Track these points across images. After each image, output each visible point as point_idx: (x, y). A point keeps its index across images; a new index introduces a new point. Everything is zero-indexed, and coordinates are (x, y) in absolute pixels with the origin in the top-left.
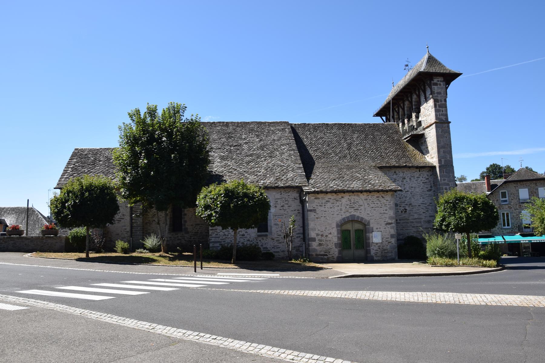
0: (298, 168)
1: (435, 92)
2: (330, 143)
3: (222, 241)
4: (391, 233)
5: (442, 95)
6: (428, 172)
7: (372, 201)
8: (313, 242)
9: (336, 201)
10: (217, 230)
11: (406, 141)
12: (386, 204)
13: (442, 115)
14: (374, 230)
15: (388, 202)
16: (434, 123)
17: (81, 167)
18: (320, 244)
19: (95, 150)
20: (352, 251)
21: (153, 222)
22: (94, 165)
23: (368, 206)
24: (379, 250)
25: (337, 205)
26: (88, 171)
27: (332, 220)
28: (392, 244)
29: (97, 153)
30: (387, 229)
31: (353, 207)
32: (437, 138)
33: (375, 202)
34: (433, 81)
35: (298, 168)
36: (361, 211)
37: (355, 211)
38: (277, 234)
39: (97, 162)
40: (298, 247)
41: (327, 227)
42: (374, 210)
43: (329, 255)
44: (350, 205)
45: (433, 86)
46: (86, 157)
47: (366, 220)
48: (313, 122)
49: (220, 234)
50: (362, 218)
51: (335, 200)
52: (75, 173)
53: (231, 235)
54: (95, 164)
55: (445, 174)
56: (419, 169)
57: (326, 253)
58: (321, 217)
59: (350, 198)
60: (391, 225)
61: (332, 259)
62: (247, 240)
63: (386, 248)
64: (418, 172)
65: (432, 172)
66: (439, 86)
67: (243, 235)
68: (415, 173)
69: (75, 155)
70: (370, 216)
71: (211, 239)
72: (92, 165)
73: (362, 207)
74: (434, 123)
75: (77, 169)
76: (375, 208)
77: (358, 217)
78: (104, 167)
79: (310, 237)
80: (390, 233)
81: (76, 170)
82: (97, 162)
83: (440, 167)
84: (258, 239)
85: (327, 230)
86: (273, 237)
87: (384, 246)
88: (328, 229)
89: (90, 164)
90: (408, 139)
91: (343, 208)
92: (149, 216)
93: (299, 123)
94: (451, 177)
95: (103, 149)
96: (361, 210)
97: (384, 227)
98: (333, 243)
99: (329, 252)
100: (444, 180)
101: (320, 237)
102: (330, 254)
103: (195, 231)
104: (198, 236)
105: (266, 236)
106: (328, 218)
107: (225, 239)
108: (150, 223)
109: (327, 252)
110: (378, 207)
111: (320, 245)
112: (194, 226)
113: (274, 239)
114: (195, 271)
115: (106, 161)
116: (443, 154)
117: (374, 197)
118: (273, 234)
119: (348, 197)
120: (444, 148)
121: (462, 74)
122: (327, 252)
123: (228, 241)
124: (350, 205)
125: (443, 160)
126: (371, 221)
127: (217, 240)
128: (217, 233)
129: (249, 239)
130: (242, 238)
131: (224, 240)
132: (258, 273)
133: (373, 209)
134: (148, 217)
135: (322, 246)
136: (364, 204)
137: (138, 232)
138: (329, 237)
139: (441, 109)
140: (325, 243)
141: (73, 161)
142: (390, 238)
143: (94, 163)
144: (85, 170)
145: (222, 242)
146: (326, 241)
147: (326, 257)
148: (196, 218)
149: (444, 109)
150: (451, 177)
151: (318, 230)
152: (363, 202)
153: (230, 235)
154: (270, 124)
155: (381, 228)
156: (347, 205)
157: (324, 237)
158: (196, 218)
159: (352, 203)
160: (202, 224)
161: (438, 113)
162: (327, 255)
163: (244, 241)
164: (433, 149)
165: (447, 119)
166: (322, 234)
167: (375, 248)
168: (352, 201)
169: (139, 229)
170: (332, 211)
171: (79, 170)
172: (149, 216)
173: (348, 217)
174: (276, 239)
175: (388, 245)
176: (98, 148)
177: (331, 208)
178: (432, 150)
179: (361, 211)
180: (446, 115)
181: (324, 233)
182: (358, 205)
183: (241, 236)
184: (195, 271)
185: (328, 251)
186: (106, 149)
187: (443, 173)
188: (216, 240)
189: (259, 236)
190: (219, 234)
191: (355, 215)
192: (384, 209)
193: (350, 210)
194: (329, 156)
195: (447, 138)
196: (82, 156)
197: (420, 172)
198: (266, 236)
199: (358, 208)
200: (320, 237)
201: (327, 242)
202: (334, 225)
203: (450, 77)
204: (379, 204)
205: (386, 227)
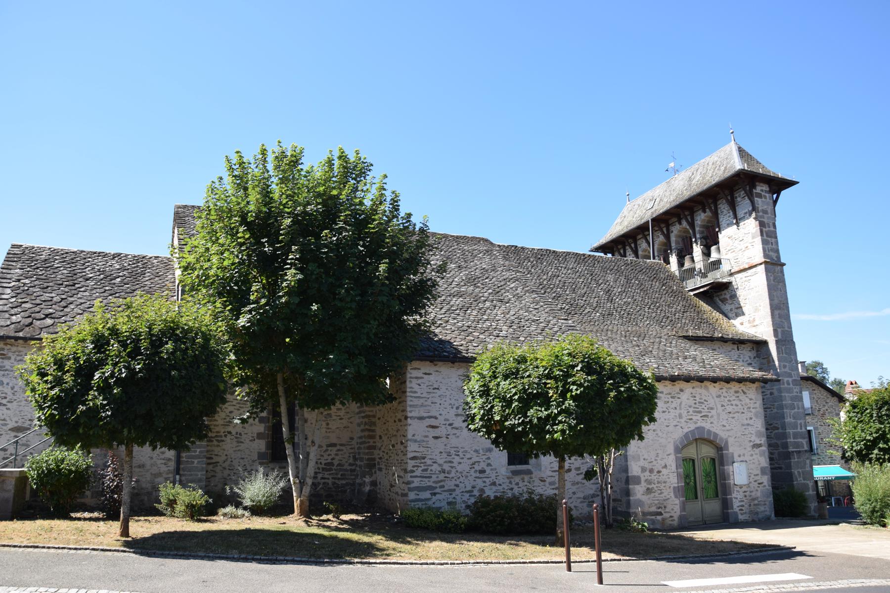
0: (570, 328)
1: (760, 209)
2: (574, 287)
3: (438, 485)
4: (762, 465)
5: (770, 215)
6: (750, 351)
7: (728, 401)
8: (636, 486)
9: (672, 397)
10: (425, 460)
11: (694, 295)
12: (749, 406)
13: (772, 250)
14: (735, 460)
15: (751, 401)
16: (761, 264)
17: (39, 290)
18: (648, 489)
19: (67, 253)
20: (700, 502)
21: (226, 436)
22: (73, 288)
23: (723, 410)
24: (746, 501)
25: (674, 405)
26: (63, 299)
27: (667, 439)
28: (765, 486)
29: (73, 261)
30: (755, 456)
31: (700, 412)
32: (768, 290)
33: (734, 403)
34: (755, 189)
35: (570, 328)
36: (712, 420)
37: (703, 420)
38: (551, 468)
39: (80, 280)
40: (592, 497)
41: (659, 452)
42: (733, 418)
43: (665, 512)
44: (694, 408)
45: (756, 199)
46: (47, 267)
47: (721, 439)
48: (529, 245)
49: (432, 468)
50: (716, 435)
51: (669, 396)
52: (27, 302)
53: (457, 471)
54: (77, 286)
55: (784, 355)
56: (736, 346)
57: (659, 508)
58: (649, 430)
59: (694, 391)
60: (760, 448)
61: (671, 522)
62: (489, 483)
63: (756, 494)
64: (736, 350)
65: (757, 351)
66: (763, 199)
67: (482, 471)
68: (732, 352)
69: (15, 259)
70: (728, 430)
71: (413, 482)
72: (67, 286)
73: (714, 412)
74: (761, 264)
75: (30, 292)
76: (734, 413)
77: (709, 432)
78: (102, 295)
79: (630, 475)
80: (759, 464)
81: (28, 295)
82: (80, 280)
83: (777, 342)
84: (512, 480)
85: (660, 458)
86: (543, 475)
87: (752, 492)
88: (660, 456)
89: (62, 284)
90: (705, 289)
91: (684, 414)
92: (216, 420)
93: (506, 245)
94: (793, 362)
95: (88, 253)
96: (712, 417)
97: (750, 453)
98: (670, 487)
99: (665, 507)
100: (785, 367)
101: (647, 473)
102: (667, 510)
103: (326, 462)
104: (334, 472)
105: (529, 472)
106: (660, 434)
107: (444, 481)
108: (219, 439)
109: (661, 508)
110: (738, 412)
111: (649, 491)
112: (325, 448)
113: (544, 481)
114: (601, 581)
115: (102, 280)
116: (780, 320)
117: (731, 391)
118: (543, 469)
119: (691, 390)
120: (780, 309)
121: (798, 183)
122: (661, 508)
123: (450, 486)
124: (694, 408)
125: (779, 330)
126: (731, 441)
127: (427, 483)
128: (426, 467)
129: (495, 480)
130: (481, 478)
131: (442, 484)
132: (721, 576)
133: (731, 415)
134: (215, 423)
135: (652, 495)
136: (716, 405)
137: (196, 461)
138: (663, 475)
139: (769, 239)
140: (657, 487)
141: (12, 271)
142: (760, 476)
143: (72, 282)
144: (52, 297)
145: (436, 487)
146: (658, 482)
147: (659, 518)
148: (328, 428)
149: (773, 240)
150: (793, 362)
151: (644, 459)
152: (715, 402)
153: (454, 471)
154: (457, 239)
155: (746, 454)
156: (690, 407)
157: (655, 473)
158: (328, 428)
159: (698, 404)
160: (341, 445)
161: (766, 247)
162: (661, 514)
163: (484, 484)
164: (756, 310)
165: (779, 257)
166: (651, 467)
167: (739, 497)
168: (697, 398)
169: (197, 453)
170: (665, 420)
171: (35, 294)
172: (216, 420)
173: (692, 432)
174: (548, 480)
175: (759, 489)
176: (75, 250)
177: (664, 412)
178: (755, 312)
179: (712, 420)
180: (777, 251)
181: (654, 466)
182: (707, 406)
183: (478, 475)
184: (601, 581)
185: (663, 503)
186: (95, 253)
187: (783, 354)
188: (423, 484)
189: (515, 473)
190: (430, 468)
191: (703, 428)
192: (748, 417)
193: (694, 418)
194: (584, 311)
195: (782, 292)
196: (36, 264)
197: (738, 350)
198: (529, 472)
199: (708, 414)
200: (647, 473)
201: (659, 485)
202: (671, 449)
203: (778, 185)
204: (740, 406)
205: (753, 453)
